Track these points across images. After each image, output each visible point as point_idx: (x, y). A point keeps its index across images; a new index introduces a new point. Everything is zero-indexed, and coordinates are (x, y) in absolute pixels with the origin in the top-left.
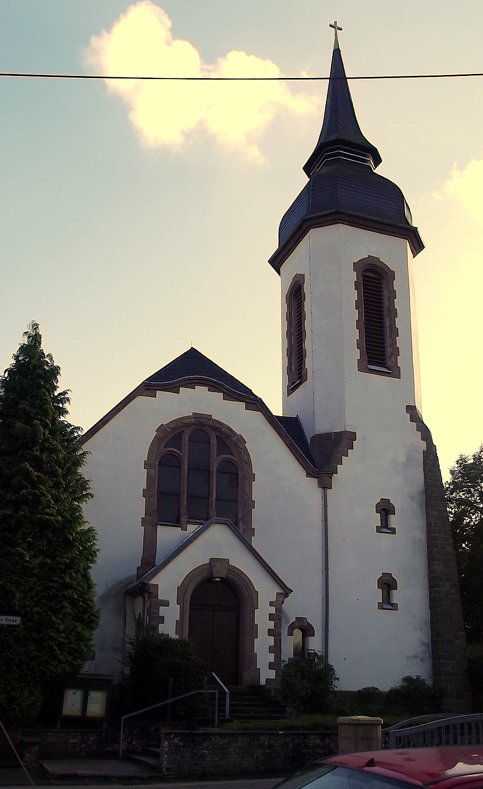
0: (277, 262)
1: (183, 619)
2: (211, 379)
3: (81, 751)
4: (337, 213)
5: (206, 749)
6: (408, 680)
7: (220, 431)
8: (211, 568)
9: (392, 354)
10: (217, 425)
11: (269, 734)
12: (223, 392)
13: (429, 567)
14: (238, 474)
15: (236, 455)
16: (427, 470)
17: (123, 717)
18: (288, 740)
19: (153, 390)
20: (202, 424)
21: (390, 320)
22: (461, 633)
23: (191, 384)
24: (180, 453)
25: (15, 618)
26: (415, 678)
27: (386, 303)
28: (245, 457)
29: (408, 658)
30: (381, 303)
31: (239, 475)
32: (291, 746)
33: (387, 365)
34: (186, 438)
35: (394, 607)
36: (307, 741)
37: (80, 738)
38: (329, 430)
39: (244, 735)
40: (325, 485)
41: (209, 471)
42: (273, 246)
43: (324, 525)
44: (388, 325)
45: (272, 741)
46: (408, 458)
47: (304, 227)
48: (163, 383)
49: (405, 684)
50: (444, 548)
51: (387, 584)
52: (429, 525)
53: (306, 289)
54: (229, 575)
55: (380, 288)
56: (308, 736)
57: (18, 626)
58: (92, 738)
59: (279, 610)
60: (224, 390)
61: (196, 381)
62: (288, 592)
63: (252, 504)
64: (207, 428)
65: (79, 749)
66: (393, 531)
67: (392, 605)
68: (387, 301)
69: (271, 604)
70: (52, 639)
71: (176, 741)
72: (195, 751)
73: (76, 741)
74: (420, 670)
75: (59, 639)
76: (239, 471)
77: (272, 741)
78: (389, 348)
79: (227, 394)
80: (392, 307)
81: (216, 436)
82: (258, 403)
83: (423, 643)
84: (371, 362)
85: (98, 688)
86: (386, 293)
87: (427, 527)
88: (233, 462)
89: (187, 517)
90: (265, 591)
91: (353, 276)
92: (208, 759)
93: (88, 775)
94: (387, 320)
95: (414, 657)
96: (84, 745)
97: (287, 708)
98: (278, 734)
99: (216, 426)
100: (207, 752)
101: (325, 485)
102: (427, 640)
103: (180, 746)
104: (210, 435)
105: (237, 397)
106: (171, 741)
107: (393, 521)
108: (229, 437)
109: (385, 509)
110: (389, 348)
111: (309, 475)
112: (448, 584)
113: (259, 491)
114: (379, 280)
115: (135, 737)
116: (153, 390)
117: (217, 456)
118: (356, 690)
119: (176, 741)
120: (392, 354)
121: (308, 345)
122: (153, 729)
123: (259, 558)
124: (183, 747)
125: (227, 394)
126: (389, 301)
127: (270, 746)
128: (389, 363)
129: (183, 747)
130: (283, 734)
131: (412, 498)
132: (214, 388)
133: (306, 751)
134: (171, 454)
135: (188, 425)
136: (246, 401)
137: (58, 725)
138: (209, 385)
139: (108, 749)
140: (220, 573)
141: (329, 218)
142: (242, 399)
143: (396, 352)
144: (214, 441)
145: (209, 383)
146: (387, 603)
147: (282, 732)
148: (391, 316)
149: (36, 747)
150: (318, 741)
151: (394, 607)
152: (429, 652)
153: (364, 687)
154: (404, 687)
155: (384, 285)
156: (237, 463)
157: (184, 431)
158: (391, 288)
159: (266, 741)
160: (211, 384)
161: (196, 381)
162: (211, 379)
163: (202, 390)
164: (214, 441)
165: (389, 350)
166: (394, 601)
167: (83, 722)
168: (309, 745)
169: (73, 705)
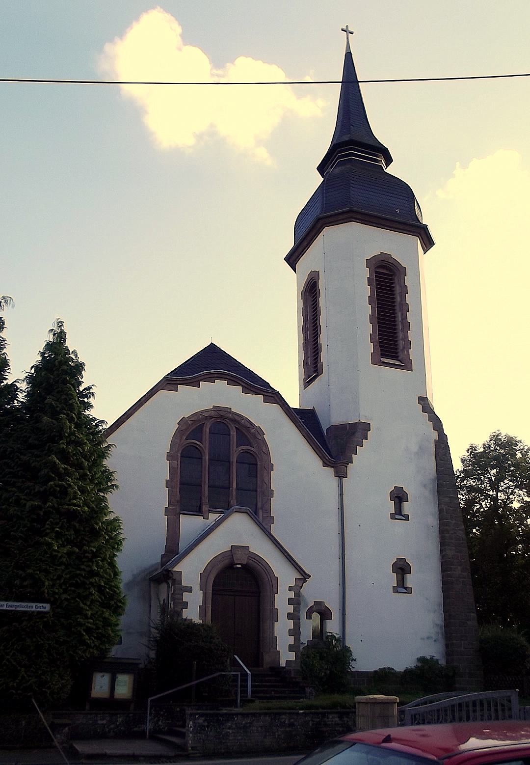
3: (109, 732)
6: (422, 660)
7: (239, 423)
9: (404, 348)
10: (237, 418)
11: (290, 713)
12: (242, 386)
13: (441, 551)
15: (255, 446)
17: (150, 699)
18: (308, 718)
20: (221, 417)
21: (402, 314)
22: (472, 614)
23: (211, 378)
24: (201, 445)
25: (44, 605)
26: (429, 658)
29: (422, 639)
30: (393, 298)
31: (258, 466)
35: (408, 590)
36: (326, 719)
37: (108, 719)
38: (344, 422)
39: (265, 714)
40: (341, 475)
41: (229, 462)
44: (400, 319)
45: (292, 720)
46: (420, 448)
47: (319, 225)
49: (419, 665)
51: (402, 569)
53: (321, 285)
54: (250, 561)
58: (120, 720)
59: (298, 595)
60: (243, 384)
61: (216, 375)
62: (306, 577)
65: (107, 730)
67: (406, 588)
69: (290, 589)
70: (81, 625)
73: (105, 722)
74: (434, 650)
76: (258, 460)
78: (401, 341)
80: (404, 302)
81: (236, 428)
82: (275, 396)
84: (383, 356)
90: (285, 576)
94: (399, 314)
95: (428, 638)
97: (306, 689)
98: (298, 713)
101: (341, 475)
102: (440, 620)
103: (204, 726)
105: (259, 391)
106: (196, 721)
107: (407, 508)
109: (399, 497)
110: (401, 341)
111: (325, 464)
112: (459, 568)
113: (278, 480)
114: (391, 276)
118: (373, 671)
119: (201, 721)
121: (323, 340)
122: (178, 709)
124: (208, 726)
126: (401, 296)
127: (291, 725)
128: (401, 356)
129: (208, 726)
130: (303, 713)
131: (425, 486)
132: (233, 381)
133: (324, 729)
134: (247, 452)
136: (264, 393)
137: (87, 707)
139: (135, 729)
140: (240, 560)
143: (408, 345)
144: (233, 433)
146: (402, 587)
147: (302, 711)
151: (408, 590)
154: (418, 667)
155: (396, 280)
157: (204, 423)
161: (216, 375)
163: (221, 384)
164: (233, 433)
165: (401, 344)
167: (111, 704)
168: (328, 723)
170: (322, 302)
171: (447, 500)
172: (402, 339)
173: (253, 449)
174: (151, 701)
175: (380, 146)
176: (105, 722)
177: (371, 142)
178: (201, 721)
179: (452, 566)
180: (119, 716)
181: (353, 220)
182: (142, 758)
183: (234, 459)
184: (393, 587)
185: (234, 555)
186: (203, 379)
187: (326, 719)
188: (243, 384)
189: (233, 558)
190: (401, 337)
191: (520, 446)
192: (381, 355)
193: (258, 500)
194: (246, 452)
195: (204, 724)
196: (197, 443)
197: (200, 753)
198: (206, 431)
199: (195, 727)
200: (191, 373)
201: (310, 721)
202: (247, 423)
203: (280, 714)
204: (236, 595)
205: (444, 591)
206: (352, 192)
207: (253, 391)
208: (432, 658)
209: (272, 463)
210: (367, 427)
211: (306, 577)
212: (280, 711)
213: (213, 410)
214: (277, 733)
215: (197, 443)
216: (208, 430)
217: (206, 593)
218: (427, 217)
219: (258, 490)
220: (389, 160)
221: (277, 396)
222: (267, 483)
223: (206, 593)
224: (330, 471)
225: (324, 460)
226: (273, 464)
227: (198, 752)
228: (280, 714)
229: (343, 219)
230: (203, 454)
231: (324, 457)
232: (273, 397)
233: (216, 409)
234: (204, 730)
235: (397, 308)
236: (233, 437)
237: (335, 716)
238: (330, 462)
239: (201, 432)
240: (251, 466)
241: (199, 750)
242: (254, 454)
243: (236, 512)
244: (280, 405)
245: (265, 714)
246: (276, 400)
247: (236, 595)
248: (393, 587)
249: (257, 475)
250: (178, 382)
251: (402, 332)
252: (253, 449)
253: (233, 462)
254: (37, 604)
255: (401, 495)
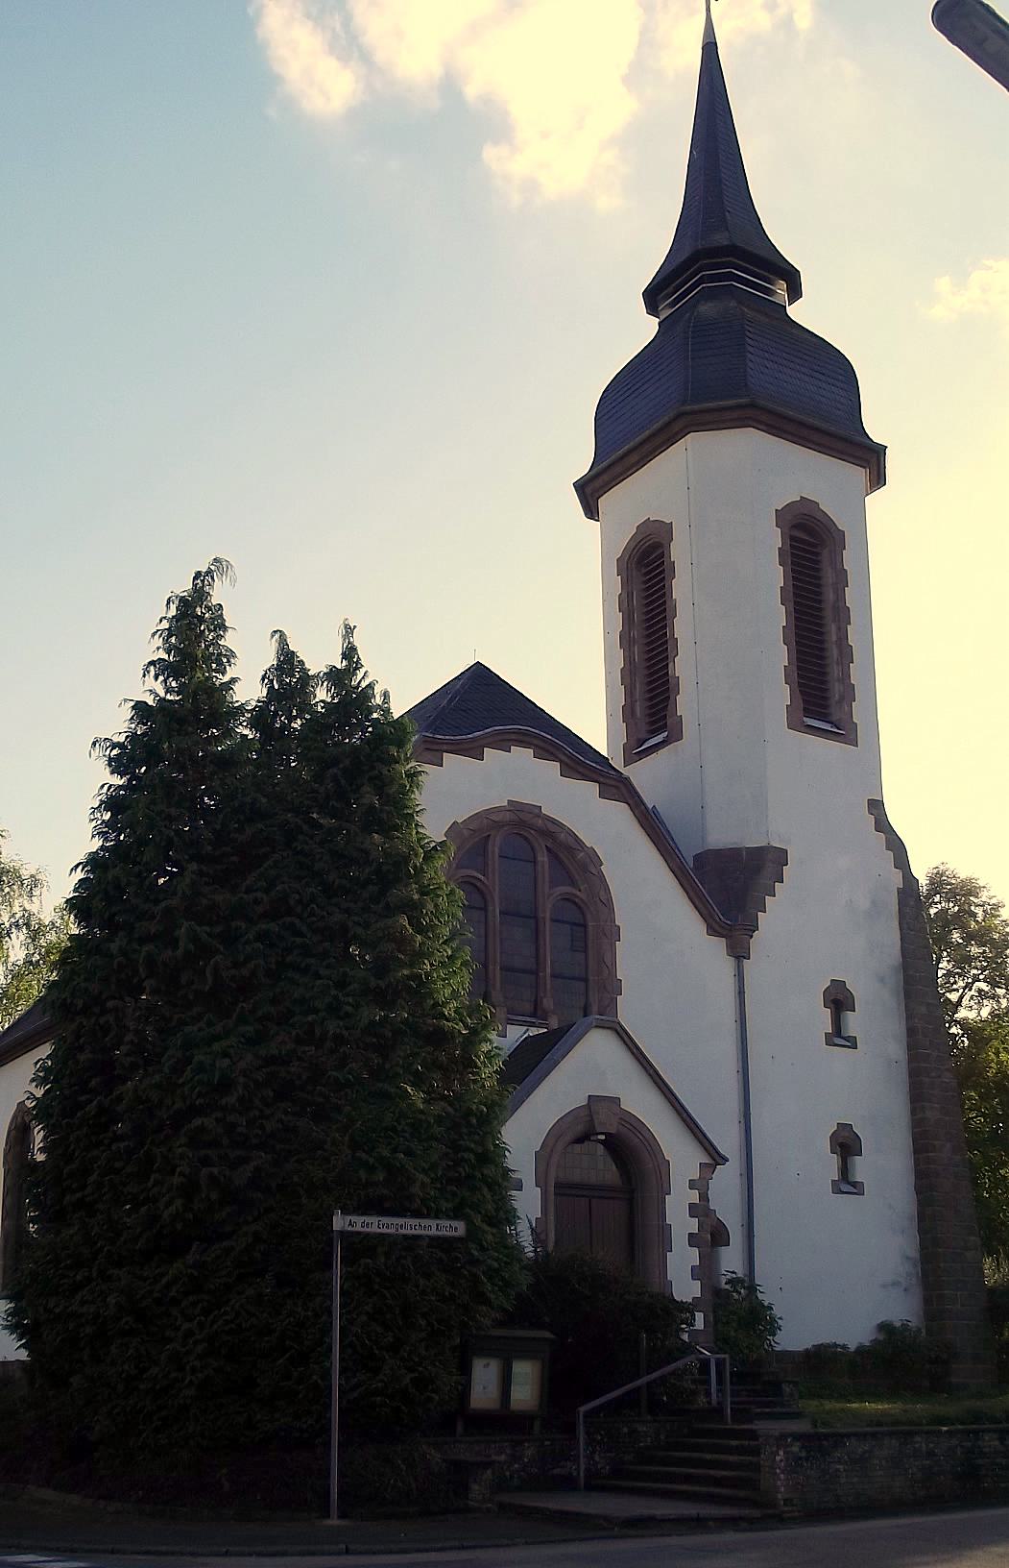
0: (590, 492)
1: (546, 1218)
2: (542, 733)
3: (511, 1477)
4: (752, 406)
5: (839, 1463)
6: (885, 1327)
8: (591, 1116)
10: (552, 828)
11: (927, 1433)
12: (561, 762)
13: (913, 1112)
14: (585, 926)
15: (582, 888)
16: (905, 926)
17: (582, 1409)
18: (954, 1442)
19: (437, 750)
20: (521, 824)
21: (839, 629)
22: (973, 1238)
23: (503, 744)
25: (455, 1224)
26: (898, 1324)
27: (830, 596)
28: (602, 893)
29: (884, 1286)
30: (820, 594)
31: (590, 929)
32: (959, 1453)
33: (834, 719)
34: (495, 848)
35: (857, 1189)
36: (980, 1443)
37: (508, 1451)
38: (736, 843)
39: (891, 1434)
40: (739, 953)
41: (536, 918)
42: (581, 457)
43: (739, 1028)
44: (834, 638)
45: (931, 1445)
46: (873, 903)
47: (676, 427)
48: (447, 737)
50: (939, 1077)
51: (846, 1145)
52: (911, 1032)
53: (679, 552)
55: (817, 562)
56: (981, 1434)
57: (460, 1239)
58: (529, 1452)
59: (704, 1197)
60: (563, 758)
61: (513, 737)
62: (720, 1161)
63: (617, 988)
64: (532, 832)
65: (508, 1473)
66: (852, 1043)
67: (854, 1184)
68: (831, 591)
69: (692, 1185)
70: (475, 1262)
71: (795, 1449)
72: (823, 1466)
73: (503, 1458)
75: (489, 1261)
76: (589, 916)
77: (931, 1445)
78: (837, 684)
79: (567, 764)
82: (621, 786)
83: (908, 1258)
84: (808, 713)
85: (525, 1355)
86: (828, 576)
87: (908, 1036)
88: (479, 884)
89: (505, 1009)
90: (681, 1158)
91: (775, 539)
92: (843, 1480)
93: (671, 1517)
94: (833, 628)
95: (895, 1284)
96: (516, 1466)
97: (783, 1385)
98: (940, 1431)
99: (497, 819)
100: (841, 1467)
101: (739, 953)
102: (912, 1249)
103: (800, 1458)
104: (536, 845)
105: (586, 772)
106: (789, 1449)
107: (853, 1023)
108: (570, 850)
109: (839, 1000)
110: (837, 684)
111: (712, 931)
112: (948, 1145)
113: (630, 961)
114: (815, 546)
115: (598, 1448)
116: (437, 750)
117: (551, 888)
120: (842, 698)
121: (683, 667)
122: (625, 1430)
123: (670, 1096)
124: (807, 1459)
125: (567, 764)
126: (836, 592)
127: (930, 1454)
129: (807, 1459)
130: (947, 1431)
131: (882, 980)
132: (545, 751)
133: (980, 1461)
134: (568, 899)
135: (498, 825)
136: (602, 780)
137: (460, 1429)
138: (534, 745)
139: (557, 1471)
141: (735, 414)
142: (594, 776)
144: (543, 858)
145: (536, 742)
146: (847, 1183)
147: (945, 1428)
148: (839, 620)
149: (489, 1472)
150: (997, 1443)
151: (857, 1189)
152: (918, 1273)
153: (816, 1343)
154: (880, 1341)
155: (825, 553)
156: (586, 904)
157: (489, 836)
158: (839, 566)
159: (924, 1445)
160: (542, 744)
161: (513, 737)
162: (542, 733)
163: (523, 756)
164: (543, 858)
165: (836, 690)
166: (859, 1176)
167: (503, 1421)
168: (984, 1450)
169: (484, 1388)
170: (681, 589)
171: (923, 1010)
172: (839, 680)
173: (578, 893)
174: (585, 1416)
175: (789, 268)
176: (503, 1458)
177: (763, 253)
178: (795, 1449)
179: (936, 1143)
180: (526, 1445)
181: (751, 423)
182: (711, 1523)
183: (546, 913)
184: (832, 1181)
185: (594, 1117)
186: (490, 744)
187: (980, 1443)
188: (563, 758)
189: (592, 1120)
190: (836, 675)
191: (984, 897)
192: (804, 709)
193: (591, 998)
194: (472, 884)
195: (800, 1454)
196: (480, 876)
197: (799, 1511)
198: (493, 852)
199: (787, 1459)
200: (467, 728)
201: (957, 1446)
202: (571, 841)
203: (911, 1434)
204: (594, 1197)
205: (919, 1190)
206: (750, 364)
207: (579, 773)
208: (905, 1326)
209: (617, 923)
210: (781, 857)
211: (720, 1161)
212: (913, 1428)
213: (508, 808)
214: (910, 1471)
215: (480, 876)
216: (497, 850)
217: (546, 1191)
218: (876, 424)
219: (591, 978)
220: (795, 292)
221: (625, 785)
222: (610, 967)
223: (546, 1191)
224: (719, 944)
225: (711, 921)
226: (619, 927)
227: (795, 1508)
228: (911, 1434)
229: (731, 420)
230: (488, 898)
231: (712, 917)
232: (617, 787)
233: (515, 807)
234: (802, 1466)
235: (828, 613)
236: (543, 866)
237: (995, 1436)
238: (720, 926)
239: (485, 853)
240: (575, 928)
241: (796, 1505)
242: (582, 905)
243: (596, 1027)
244: (629, 805)
245: (891, 1434)
246: (623, 795)
247: (594, 1197)
248: (832, 1181)
249: (586, 946)
250: (445, 747)
251: (838, 664)
252: (578, 893)
253: (544, 918)
254: (438, 1222)
255: (840, 997)
